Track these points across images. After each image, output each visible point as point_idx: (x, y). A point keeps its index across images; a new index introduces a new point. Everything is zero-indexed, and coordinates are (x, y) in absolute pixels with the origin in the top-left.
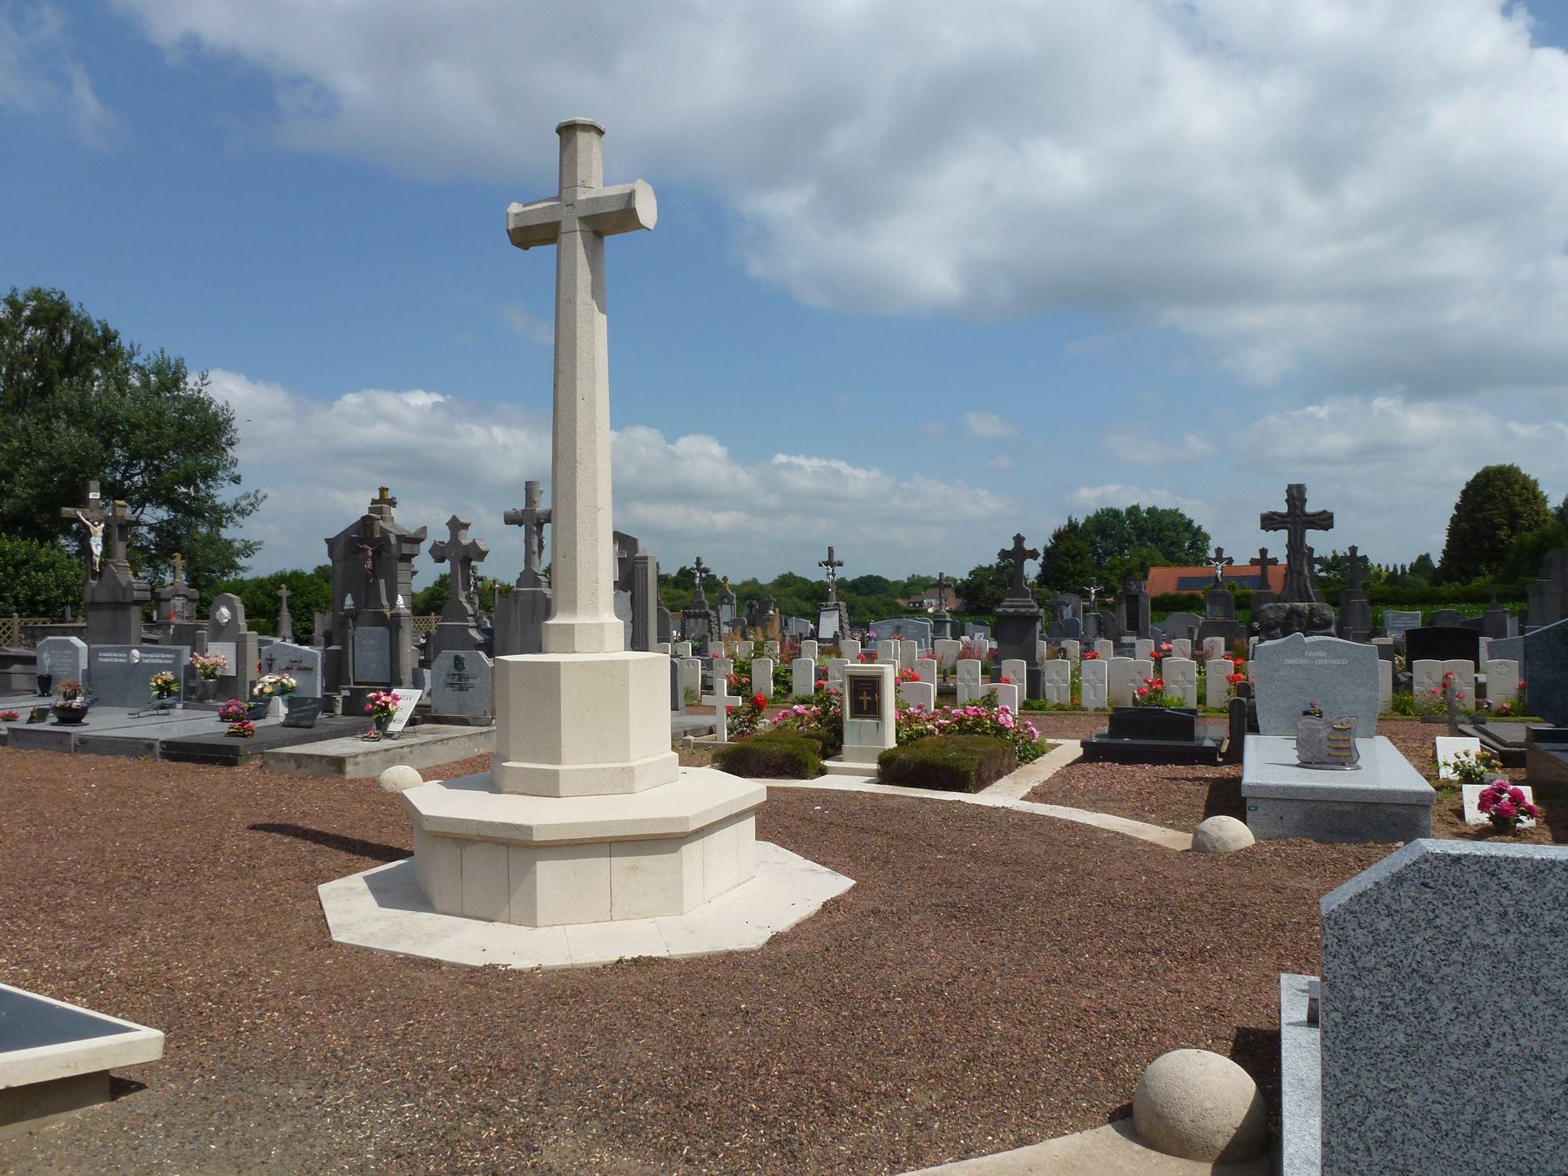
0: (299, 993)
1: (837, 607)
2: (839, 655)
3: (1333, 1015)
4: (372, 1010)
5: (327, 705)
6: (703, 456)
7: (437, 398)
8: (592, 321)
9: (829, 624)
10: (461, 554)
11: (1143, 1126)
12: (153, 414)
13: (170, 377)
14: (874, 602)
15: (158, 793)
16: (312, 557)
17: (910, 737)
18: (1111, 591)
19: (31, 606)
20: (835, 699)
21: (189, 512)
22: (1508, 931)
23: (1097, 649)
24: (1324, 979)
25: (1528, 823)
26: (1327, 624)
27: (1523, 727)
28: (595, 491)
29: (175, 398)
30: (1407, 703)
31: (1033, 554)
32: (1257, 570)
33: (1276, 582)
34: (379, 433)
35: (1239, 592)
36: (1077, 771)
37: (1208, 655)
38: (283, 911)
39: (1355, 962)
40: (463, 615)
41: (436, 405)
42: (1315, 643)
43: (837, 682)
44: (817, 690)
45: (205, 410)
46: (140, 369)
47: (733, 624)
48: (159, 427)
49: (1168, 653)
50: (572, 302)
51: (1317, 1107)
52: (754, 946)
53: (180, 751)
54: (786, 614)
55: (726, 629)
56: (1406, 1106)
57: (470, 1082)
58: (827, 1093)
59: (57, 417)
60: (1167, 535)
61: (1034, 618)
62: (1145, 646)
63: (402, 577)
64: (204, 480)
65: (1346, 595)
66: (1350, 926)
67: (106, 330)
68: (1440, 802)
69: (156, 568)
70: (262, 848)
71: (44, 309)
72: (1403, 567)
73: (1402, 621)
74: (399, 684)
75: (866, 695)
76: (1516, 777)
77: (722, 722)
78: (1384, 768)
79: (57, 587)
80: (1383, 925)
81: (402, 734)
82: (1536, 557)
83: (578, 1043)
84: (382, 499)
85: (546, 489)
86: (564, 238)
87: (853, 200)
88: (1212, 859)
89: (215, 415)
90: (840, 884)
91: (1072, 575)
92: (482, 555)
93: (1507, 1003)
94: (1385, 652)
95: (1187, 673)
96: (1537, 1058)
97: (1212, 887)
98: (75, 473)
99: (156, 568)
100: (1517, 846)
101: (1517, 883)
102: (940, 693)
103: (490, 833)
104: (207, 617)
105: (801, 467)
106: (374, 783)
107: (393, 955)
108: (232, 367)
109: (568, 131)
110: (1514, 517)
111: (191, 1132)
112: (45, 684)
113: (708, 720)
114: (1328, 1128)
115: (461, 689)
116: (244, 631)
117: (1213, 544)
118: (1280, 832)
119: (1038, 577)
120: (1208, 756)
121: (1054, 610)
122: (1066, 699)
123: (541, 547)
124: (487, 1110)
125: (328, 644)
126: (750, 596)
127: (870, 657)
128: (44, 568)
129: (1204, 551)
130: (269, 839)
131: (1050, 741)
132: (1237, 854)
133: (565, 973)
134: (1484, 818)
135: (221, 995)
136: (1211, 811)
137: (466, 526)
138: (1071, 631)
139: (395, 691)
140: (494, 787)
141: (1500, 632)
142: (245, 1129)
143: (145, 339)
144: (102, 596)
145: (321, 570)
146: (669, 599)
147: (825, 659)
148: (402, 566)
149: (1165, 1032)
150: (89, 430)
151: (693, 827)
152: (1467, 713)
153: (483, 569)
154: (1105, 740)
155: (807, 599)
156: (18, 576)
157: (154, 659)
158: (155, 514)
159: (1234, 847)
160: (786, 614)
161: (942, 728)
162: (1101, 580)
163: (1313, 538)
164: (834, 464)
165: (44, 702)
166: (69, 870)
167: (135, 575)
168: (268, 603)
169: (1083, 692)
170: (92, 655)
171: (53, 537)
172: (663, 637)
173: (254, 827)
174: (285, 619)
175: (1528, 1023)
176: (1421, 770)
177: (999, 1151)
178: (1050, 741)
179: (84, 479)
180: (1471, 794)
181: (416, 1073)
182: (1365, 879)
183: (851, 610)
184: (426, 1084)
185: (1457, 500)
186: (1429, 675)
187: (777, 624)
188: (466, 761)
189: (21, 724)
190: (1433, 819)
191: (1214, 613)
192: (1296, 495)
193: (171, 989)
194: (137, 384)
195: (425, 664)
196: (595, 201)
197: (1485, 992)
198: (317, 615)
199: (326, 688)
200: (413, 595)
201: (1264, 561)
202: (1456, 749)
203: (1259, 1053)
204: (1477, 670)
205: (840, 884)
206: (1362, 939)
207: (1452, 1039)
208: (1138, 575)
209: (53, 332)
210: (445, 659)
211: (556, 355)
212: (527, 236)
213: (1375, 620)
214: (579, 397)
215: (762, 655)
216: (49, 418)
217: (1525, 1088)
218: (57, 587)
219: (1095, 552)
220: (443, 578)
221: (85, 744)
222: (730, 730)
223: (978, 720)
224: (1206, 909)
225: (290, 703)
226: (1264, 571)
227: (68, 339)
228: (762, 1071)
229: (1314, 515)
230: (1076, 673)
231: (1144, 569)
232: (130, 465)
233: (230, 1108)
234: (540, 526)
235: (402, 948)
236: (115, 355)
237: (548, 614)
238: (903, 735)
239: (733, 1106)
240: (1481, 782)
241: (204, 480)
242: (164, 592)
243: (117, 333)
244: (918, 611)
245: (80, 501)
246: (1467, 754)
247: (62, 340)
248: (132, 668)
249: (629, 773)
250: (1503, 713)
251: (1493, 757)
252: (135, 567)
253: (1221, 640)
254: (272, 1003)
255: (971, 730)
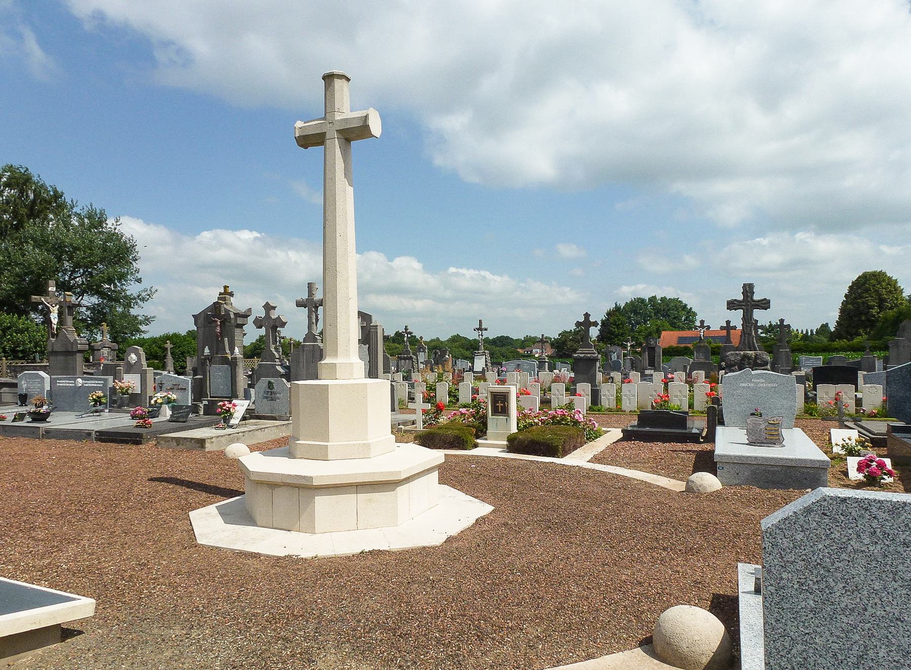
0: (177, 574)
1: (484, 354)
2: (485, 380)
3: (770, 588)
4: (220, 582)
5: (195, 409)
6: (408, 269)
7: (256, 234)
8: (345, 191)
9: (480, 363)
10: (272, 324)
11: (659, 649)
12: (87, 242)
13: (96, 220)
14: (504, 350)
15: (93, 461)
16: (185, 326)
17: (525, 426)
18: (640, 345)
19: (14, 353)
20: (482, 405)
21: (111, 299)
22: (876, 543)
23: (631, 377)
24: (764, 567)
25: (888, 480)
26: (766, 363)
27: (885, 424)
28: (347, 288)
29: (100, 233)
30: (813, 409)
31: (595, 324)
32: (724, 333)
33: (735, 340)
34: (223, 255)
35: (714, 345)
36: (620, 445)
37: (695, 381)
38: (169, 527)
39: (782, 558)
40: (273, 357)
41: (256, 238)
42: (758, 374)
43: (484, 396)
44: (473, 400)
45: (119, 240)
46: (77, 214)
47: (426, 363)
48: (91, 249)
49: (672, 379)
50: (333, 179)
51: (761, 641)
52: (438, 544)
53: (106, 437)
54: (456, 358)
55: (421, 366)
56: (816, 644)
57: (276, 623)
58: (478, 627)
59: (27, 242)
60: (672, 313)
61: (595, 360)
62: (658, 376)
63: (237, 337)
64: (120, 280)
65: (778, 347)
66: (779, 537)
67: (55, 191)
68: (833, 466)
69: (91, 331)
70: (156, 491)
71: (15, 178)
72: (812, 331)
73: (810, 362)
74: (237, 397)
75: (500, 403)
76: (881, 453)
77: (419, 417)
78: (798, 446)
79: (30, 342)
80: (799, 537)
81: (238, 426)
82: (895, 325)
83: (337, 599)
84: (226, 293)
85: (319, 287)
86: (328, 142)
87: (493, 121)
88: (697, 497)
89: (125, 243)
90: (486, 509)
91: (617, 336)
92: (283, 324)
93: (877, 586)
94: (800, 380)
95: (683, 391)
96: (897, 619)
97: (698, 511)
98: (39, 276)
99: (91, 331)
100: (882, 493)
101: (882, 515)
102: (542, 402)
103: (288, 481)
104: (123, 360)
105: (464, 275)
106: (223, 453)
107: (232, 550)
108: (134, 215)
109: (329, 78)
110: (881, 302)
111: (110, 658)
112: (23, 399)
113: (411, 417)
114: (768, 654)
115: (272, 400)
116: (145, 367)
117: (699, 318)
118: (737, 482)
119: (598, 337)
120: (695, 439)
121: (607, 355)
122: (613, 405)
123: (317, 320)
124: (286, 639)
125: (195, 375)
126: (435, 348)
127: (503, 382)
128: (21, 331)
129: (694, 322)
130: (160, 486)
131: (604, 429)
132: (711, 494)
133: (331, 560)
134: (861, 476)
135: (131, 576)
136: (696, 469)
137: (274, 308)
138: (616, 367)
139: (234, 401)
140: (291, 455)
141: (871, 368)
142: (143, 655)
143: (80, 197)
144: (58, 348)
145: (190, 333)
146: (390, 349)
147: (477, 382)
148: (237, 331)
149: (671, 595)
150: (47, 250)
151: (403, 477)
152: (850, 415)
153: (284, 332)
154: (635, 429)
155: (467, 349)
156: (5, 336)
157: (90, 384)
158: (90, 300)
159: (709, 490)
160: (456, 358)
161: (543, 422)
162: (633, 338)
163: (758, 314)
164: (483, 273)
165: (23, 410)
166: (38, 507)
167: (79, 335)
168: (160, 353)
169: (623, 402)
170: (52, 382)
171: (27, 313)
172: (387, 370)
173: (151, 480)
174: (170, 360)
175: (891, 598)
176: (821, 448)
177: (576, 662)
178: (604, 429)
179: (45, 279)
180: (853, 463)
181: (245, 618)
182: (788, 510)
183: (492, 355)
184: (251, 625)
185: (847, 292)
186: (827, 393)
187: (450, 363)
188: (275, 441)
189: (8, 422)
190: (829, 476)
191: (698, 357)
192: (748, 289)
193: (101, 575)
194: (77, 224)
195: (251, 386)
196: (346, 120)
197: (862, 578)
198: (188, 358)
199: (194, 400)
200: (244, 347)
201: (728, 327)
202: (842, 436)
203: (726, 608)
204: (856, 390)
205: (486, 509)
206: (786, 544)
207: (843, 605)
208: (655, 336)
209: (22, 192)
210: (263, 383)
211: (325, 210)
212: (308, 141)
213: (794, 361)
214: (338, 235)
215: (442, 380)
216: (22, 243)
217: (890, 637)
218: (30, 342)
219: (630, 323)
220: (261, 337)
221: (49, 434)
222: (424, 423)
223: (563, 418)
224: (694, 525)
225: (173, 409)
226: (728, 333)
227: (32, 196)
228: (442, 615)
229: (759, 301)
230: (619, 390)
231: (658, 332)
232: (73, 272)
233: (134, 643)
234: (316, 308)
235: (239, 546)
236: (62, 206)
237: (321, 357)
238: (521, 425)
239: (425, 634)
240: (859, 455)
241: (120, 280)
242: (96, 345)
243: (63, 193)
244: (530, 356)
245: (43, 292)
246: (849, 439)
247: (28, 196)
248: (77, 390)
249: (367, 446)
250: (872, 416)
251: (866, 441)
252: (78, 331)
253: (703, 373)
254: (161, 580)
255: (559, 423)
